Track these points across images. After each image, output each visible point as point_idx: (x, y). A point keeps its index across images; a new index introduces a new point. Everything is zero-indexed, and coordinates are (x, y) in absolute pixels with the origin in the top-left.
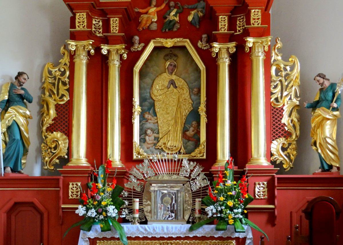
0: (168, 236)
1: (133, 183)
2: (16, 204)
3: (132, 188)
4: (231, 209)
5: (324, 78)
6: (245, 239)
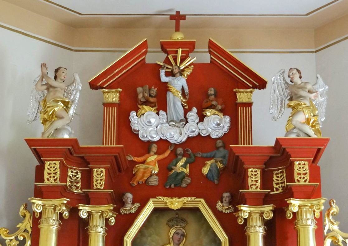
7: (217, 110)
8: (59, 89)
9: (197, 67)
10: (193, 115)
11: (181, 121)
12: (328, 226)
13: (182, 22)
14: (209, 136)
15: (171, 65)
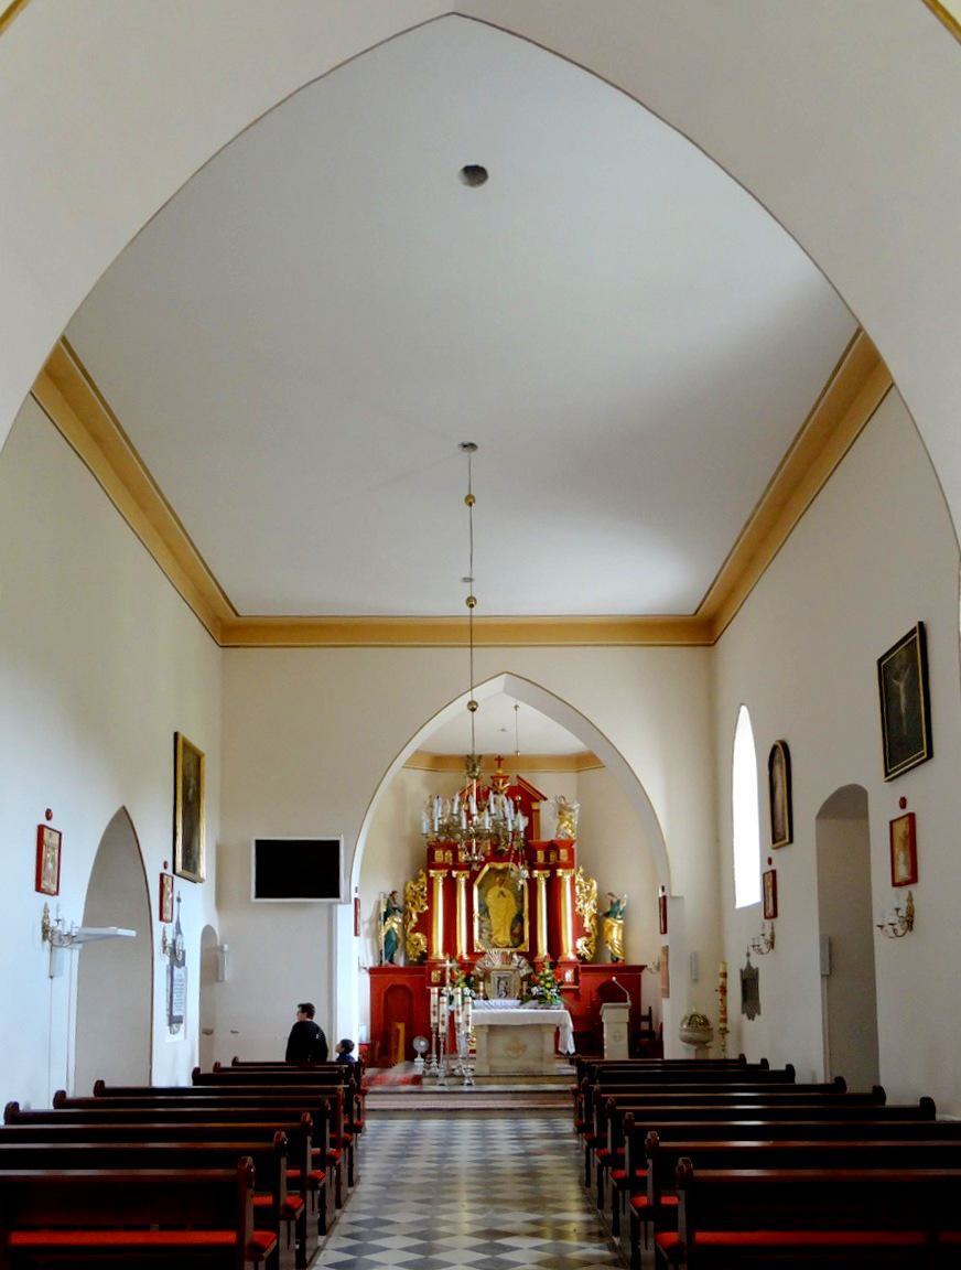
4: (549, 990)
12: (577, 880)
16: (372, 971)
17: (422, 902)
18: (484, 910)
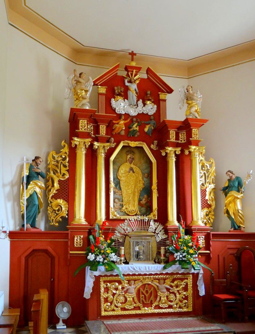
0: (149, 273)
1: (117, 235)
2: (34, 251)
3: (117, 239)
5: (232, 174)
6: (198, 274)
7: (151, 102)
8: (82, 84)
9: (142, 80)
10: (140, 102)
11: (135, 105)
13: (134, 56)
14: (147, 114)
15: (130, 77)
16: (12, 235)
17: (64, 170)
18: (118, 183)
